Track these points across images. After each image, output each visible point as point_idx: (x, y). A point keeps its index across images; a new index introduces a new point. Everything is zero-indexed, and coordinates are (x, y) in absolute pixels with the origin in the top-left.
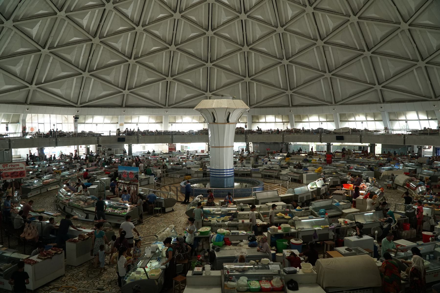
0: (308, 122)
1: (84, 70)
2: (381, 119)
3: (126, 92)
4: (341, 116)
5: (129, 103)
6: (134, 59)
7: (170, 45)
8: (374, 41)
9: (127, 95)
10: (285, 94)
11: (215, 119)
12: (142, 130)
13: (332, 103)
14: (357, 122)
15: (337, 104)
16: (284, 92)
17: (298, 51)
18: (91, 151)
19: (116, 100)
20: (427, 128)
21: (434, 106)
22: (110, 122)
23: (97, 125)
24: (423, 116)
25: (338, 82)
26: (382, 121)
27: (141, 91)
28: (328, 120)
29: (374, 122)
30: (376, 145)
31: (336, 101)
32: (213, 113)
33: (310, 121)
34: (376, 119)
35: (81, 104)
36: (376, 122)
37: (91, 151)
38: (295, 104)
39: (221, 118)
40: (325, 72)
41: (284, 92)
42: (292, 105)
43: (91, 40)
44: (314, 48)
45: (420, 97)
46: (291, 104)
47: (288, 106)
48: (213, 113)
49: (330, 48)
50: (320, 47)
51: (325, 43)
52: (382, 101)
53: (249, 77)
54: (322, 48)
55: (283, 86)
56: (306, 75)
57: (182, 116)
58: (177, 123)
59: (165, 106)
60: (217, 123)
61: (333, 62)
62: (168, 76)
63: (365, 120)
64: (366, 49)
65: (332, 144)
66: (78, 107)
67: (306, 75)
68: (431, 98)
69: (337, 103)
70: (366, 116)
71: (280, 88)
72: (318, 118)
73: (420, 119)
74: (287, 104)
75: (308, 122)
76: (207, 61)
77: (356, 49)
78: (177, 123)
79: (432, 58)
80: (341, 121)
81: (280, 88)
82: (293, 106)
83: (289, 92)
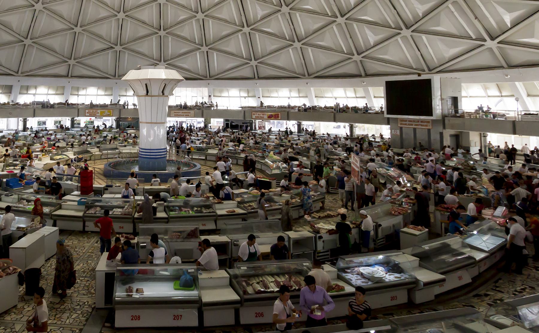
0: (85, 95)
1: (343, 15)
2: (364, 95)
3: (72, 62)
4: (22, 87)
5: (76, 73)
6: (81, 27)
7: (119, 13)
8: (347, 7)
9: (73, 65)
10: (249, 65)
11: (147, 92)
12: (350, 105)
13: (305, 76)
14: (230, 98)
15: (311, 77)
16: (248, 63)
17: (260, 18)
18: (489, 142)
19: (246, 72)
20: (341, 106)
21: (257, 84)
22: (104, 94)
23: (336, 99)
24: (101, 92)
25: (215, 56)
26: (364, 97)
27: (90, 61)
28: (106, 94)
29: (298, 99)
30: (28, 120)
31: (310, 74)
32: (165, 85)
33: (230, 96)
34: (249, 95)
35: (22, 73)
36: (358, 99)
37: (489, 142)
38: (261, 75)
39: (155, 90)
40: (202, 46)
41: (248, 63)
42: (258, 77)
43: (34, 6)
44: (279, 15)
45: (409, 69)
46: (257, 77)
47: (254, 78)
48: (165, 85)
49: (298, 15)
50: (200, 19)
51: (290, 9)
52: (363, 74)
53: (121, 45)
54: (288, 15)
55: (347, 51)
56: (272, 45)
57: (228, 89)
58: (222, 97)
59: (17, 72)
60: (152, 96)
61: (302, 31)
62: (117, 45)
63: (298, 96)
64: (338, 15)
65: (76, 119)
66: (19, 76)
67: (272, 45)
68: (424, 71)
69: (212, 77)
70: (240, 90)
71: (242, 58)
72: (288, 92)
73: (348, 96)
74: (252, 76)
75: (85, 95)
76: (159, 29)
77: (327, 15)
78: (222, 97)
79: (420, 24)
80: (71, 94)
81: (242, 58)
82: (259, 78)
83: (254, 63)
